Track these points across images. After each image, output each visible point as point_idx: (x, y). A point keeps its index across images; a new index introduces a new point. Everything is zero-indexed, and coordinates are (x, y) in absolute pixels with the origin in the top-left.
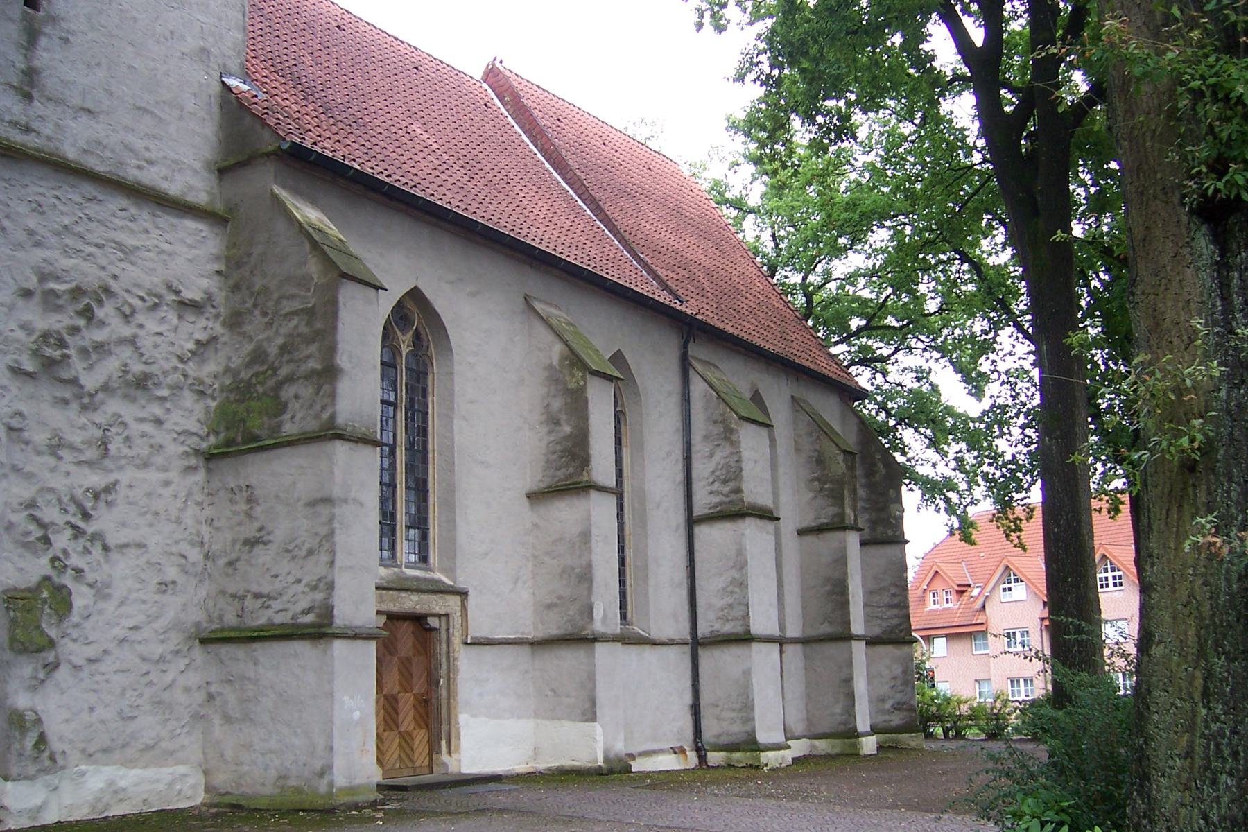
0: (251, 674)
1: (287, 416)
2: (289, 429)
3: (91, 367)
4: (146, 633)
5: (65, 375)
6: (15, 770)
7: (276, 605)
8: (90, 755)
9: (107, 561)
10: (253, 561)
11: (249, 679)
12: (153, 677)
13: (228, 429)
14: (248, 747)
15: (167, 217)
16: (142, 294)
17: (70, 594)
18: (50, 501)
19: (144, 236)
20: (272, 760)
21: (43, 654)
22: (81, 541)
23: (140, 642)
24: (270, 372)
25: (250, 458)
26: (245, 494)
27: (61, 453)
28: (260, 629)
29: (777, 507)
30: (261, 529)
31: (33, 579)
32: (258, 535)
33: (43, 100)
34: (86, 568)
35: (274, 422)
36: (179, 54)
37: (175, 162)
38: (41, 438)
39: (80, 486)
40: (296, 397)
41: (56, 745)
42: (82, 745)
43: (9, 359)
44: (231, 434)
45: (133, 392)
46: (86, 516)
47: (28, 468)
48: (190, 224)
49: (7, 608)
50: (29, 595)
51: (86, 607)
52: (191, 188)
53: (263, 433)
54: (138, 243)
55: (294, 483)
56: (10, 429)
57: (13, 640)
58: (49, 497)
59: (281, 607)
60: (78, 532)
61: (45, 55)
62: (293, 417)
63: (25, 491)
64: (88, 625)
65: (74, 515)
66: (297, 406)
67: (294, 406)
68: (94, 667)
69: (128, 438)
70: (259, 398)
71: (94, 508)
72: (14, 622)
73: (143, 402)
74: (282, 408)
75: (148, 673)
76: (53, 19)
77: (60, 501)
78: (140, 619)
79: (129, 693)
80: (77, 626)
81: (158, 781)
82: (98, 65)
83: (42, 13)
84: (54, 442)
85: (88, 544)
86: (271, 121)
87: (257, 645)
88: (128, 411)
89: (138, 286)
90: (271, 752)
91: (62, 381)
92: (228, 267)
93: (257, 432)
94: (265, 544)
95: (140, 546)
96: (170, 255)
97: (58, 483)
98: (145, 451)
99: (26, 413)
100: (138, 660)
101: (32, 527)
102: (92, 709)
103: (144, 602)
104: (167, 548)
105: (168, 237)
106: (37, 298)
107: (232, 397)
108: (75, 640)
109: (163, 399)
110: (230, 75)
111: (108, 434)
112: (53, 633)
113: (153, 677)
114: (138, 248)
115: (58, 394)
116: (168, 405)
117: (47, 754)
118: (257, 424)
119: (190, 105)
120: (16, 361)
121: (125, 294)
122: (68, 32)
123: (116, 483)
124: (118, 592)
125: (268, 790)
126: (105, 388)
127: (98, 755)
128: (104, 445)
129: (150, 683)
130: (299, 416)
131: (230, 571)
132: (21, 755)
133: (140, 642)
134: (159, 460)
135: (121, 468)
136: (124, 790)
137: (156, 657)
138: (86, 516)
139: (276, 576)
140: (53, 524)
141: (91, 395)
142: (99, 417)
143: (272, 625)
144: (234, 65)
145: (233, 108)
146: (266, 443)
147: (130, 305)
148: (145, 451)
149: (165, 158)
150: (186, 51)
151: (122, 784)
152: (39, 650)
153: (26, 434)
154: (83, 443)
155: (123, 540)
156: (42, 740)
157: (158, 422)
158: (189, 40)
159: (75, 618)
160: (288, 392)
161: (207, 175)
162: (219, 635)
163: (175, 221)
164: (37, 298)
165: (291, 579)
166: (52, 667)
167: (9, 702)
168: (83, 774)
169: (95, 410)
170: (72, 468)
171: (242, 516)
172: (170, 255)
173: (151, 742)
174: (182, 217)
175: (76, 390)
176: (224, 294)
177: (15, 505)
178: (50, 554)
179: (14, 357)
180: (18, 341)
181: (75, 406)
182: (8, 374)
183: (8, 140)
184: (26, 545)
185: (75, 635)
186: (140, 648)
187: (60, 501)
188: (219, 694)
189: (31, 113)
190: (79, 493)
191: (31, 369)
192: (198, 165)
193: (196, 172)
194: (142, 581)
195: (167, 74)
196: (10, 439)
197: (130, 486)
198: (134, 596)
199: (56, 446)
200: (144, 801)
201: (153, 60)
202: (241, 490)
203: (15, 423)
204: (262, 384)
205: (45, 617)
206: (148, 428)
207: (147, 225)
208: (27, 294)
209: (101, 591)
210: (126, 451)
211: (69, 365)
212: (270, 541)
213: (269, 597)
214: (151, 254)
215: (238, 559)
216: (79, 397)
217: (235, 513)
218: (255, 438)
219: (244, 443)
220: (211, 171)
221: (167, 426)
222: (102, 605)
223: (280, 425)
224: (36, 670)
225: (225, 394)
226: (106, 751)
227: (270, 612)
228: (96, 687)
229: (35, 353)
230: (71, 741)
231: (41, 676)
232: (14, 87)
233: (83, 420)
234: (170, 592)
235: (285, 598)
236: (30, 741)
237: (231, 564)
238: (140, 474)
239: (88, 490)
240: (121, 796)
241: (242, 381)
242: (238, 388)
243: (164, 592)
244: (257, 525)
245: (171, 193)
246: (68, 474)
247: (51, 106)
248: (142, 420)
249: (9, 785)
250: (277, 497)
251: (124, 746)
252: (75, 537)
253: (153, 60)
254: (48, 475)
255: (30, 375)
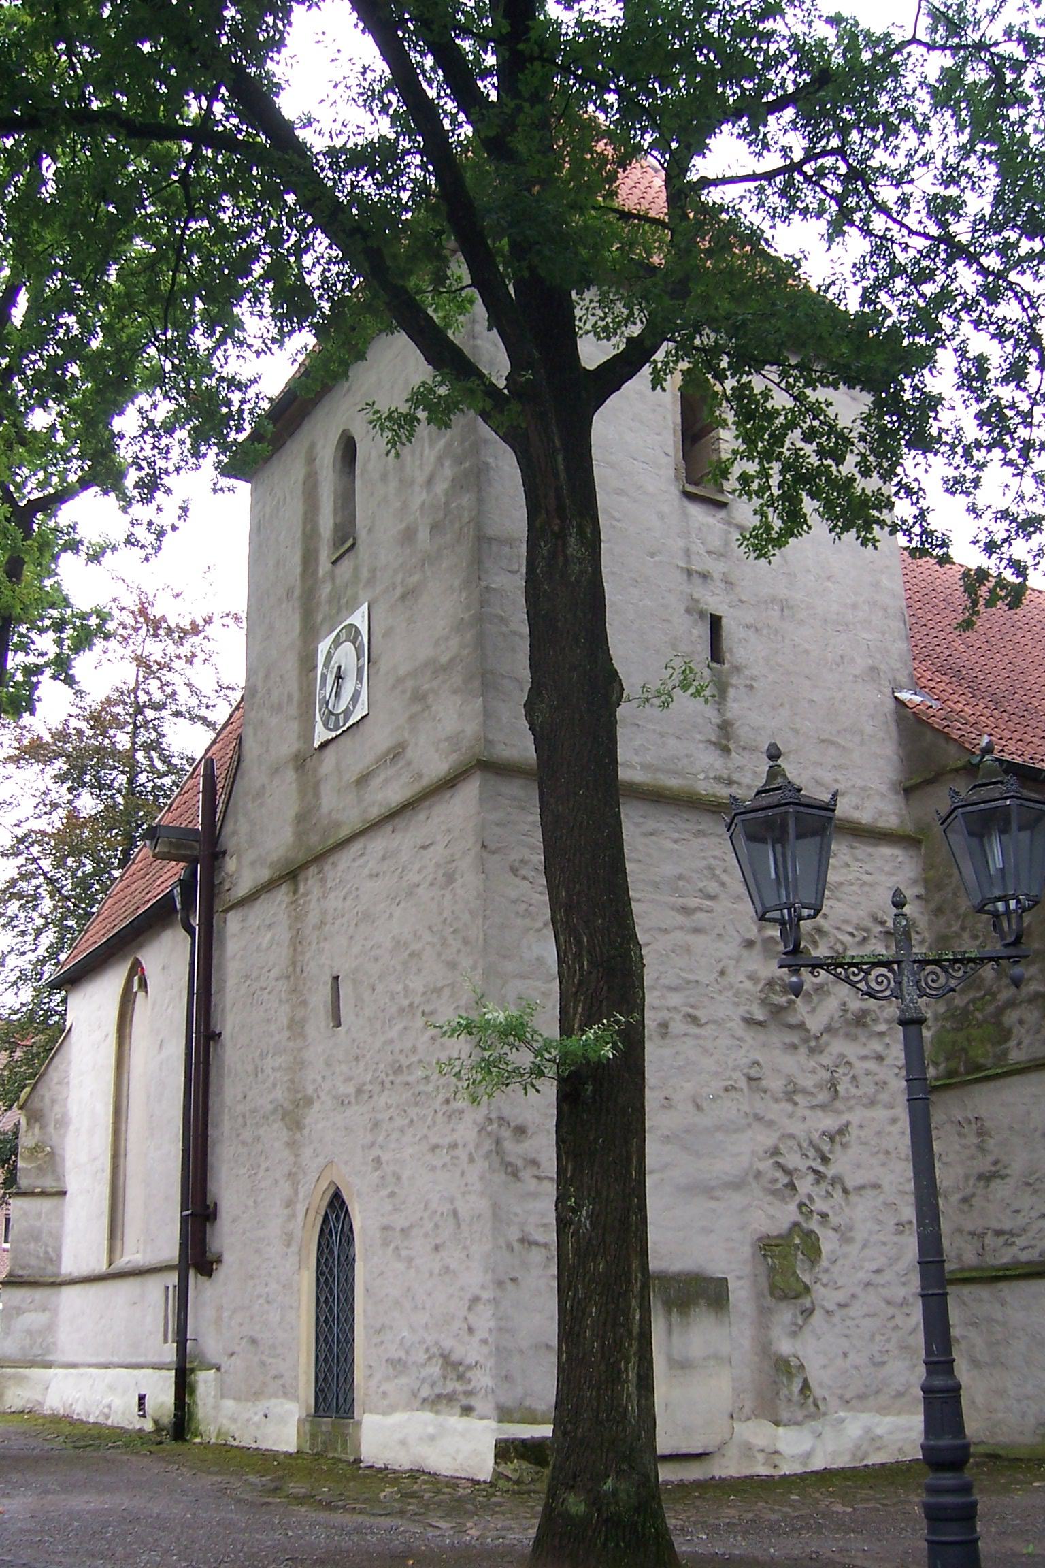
0: (999, 1316)
1: (1012, 1043)
2: (1016, 1056)
3: (814, 1010)
4: (888, 1276)
5: (793, 1020)
6: (785, 1415)
7: (1020, 1242)
8: (847, 1402)
9: (848, 1204)
10: (991, 1197)
11: (996, 1321)
12: (899, 1320)
13: (947, 1059)
14: (1001, 1393)
15: (863, 847)
16: (851, 930)
17: (818, 1239)
18: (791, 1148)
19: (844, 871)
20: (1028, 1406)
21: (800, 1301)
22: (824, 1185)
23: (883, 1286)
24: (988, 997)
25: (977, 1088)
26: (974, 1127)
27: (797, 1098)
28: (1005, 1267)
29: (684, 509)
30: (996, 1163)
31: (784, 1226)
32: (993, 1169)
33: (740, 751)
34: (830, 1214)
35: (999, 1049)
36: (851, 678)
37: (863, 789)
38: (776, 1084)
39: (817, 1131)
40: (1021, 1022)
41: (817, 1391)
42: (839, 1392)
43: (742, 1010)
44: (952, 1065)
45: (853, 1030)
46: (825, 1160)
47: (769, 1116)
48: (886, 851)
49: (764, 1255)
50: (781, 1242)
51: (833, 1252)
52: (881, 813)
53: (988, 1062)
54: (842, 879)
55: (1029, 1113)
56: (750, 1079)
57: (773, 1288)
58: (791, 1143)
59: (1026, 1244)
60: (819, 1176)
61: (736, 706)
62: (1019, 1044)
63: (767, 1139)
64: (835, 1269)
65: (814, 1159)
66: (1023, 1031)
67: (1019, 1031)
68: (844, 1312)
69: (854, 1078)
70: (979, 1025)
71: (831, 1152)
72: (772, 1269)
73: (864, 1040)
74: (1006, 1034)
75: (893, 1317)
76: (737, 669)
77: (800, 1146)
78: (881, 1262)
79: (878, 1337)
80: (827, 1271)
81: (910, 1429)
82: (782, 705)
83: (726, 666)
84: (791, 1088)
85: (830, 1188)
86: (955, 735)
87: (1001, 1285)
88: (851, 1050)
89: (846, 922)
90: (1028, 1398)
91: (791, 1027)
92: (926, 889)
93: (982, 1061)
94: (1003, 1177)
95: (876, 1186)
96: (871, 885)
97: (797, 1128)
98: (871, 1090)
99: (761, 1061)
100: (883, 1305)
101: (779, 1174)
102: (845, 1355)
103: (884, 1244)
104: (901, 1187)
105: (867, 867)
106: (758, 947)
107: (948, 1025)
108: (825, 1285)
109: (881, 1034)
110: (901, 689)
111: (836, 1075)
112: (806, 1278)
113: (899, 1320)
114: (841, 884)
115: (787, 1040)
116: (887, 1040)
117: (811, 1399)
118: (982, 1053)
119: (869, 729)
120: (749, 1012)
121: (836, 932)
122: (752, 679)
123: (848, 1124)
124: (859, 1236)
125: (1028, 1439)
126: (829, 1029)
127: (854, 1402)
128: (833, 1085)
129: (897, 1327)
130: (1026, 1041)
131: (966, 1208)
132: (789, 1400)
133: (883, 1286)
134: (884, 1097)
135: (850, 1109)
136: (880, 1437)
137: (899, 1300)
138: (825, 1160)
139: (1018, 1211)
140: (796, 1169)
141: (817, 1038)
142: (826, 1059)
143: (1017, 1264)
144: (903, 678)
145: (912, 726)
146: (992, 1072)
147: (842, 943)
148: (871, 1090)
149: (853, 786)
150: (857, 672)
151: (879, 1431)
152: (797, 1297)
153: (764, 1083)
154: (815, 1086)
155: (860, 1182)
156: (806, 1386)
157: (880, 1058)
158: (859, 661)
159: (824, 1263)
160: (1011, 1017)
161: (894, 797)
162: (959, 1276)
163: (870, 850)
164: (758, 947)
165: (1034, 1214)
166: (808, 1313)
167: (773, 1348)
168: (842, 1421)
169: (822, 1052)
170: (807, 1113)
171: (973, 1150)
172: (871, 885)
173: (902, 1389)
174: (876, 845)
175: (803, 1034)
176: (926, 918)
177: (761, 1153)
178: (797, 1200)
179: (747, 1007)
180: (747, 991)
181: (803, 1050)
182: (742, 1024)
183: (715, 796)
184: (774, 1193)
185: (825, 1281)
186: (885, 1292)
187: (800, 1146)
188: (964, 1337)
189: (730, 765)
190: (816, 1136)
191: (761, 1018)
192: (883, 788)
193: (883, 795)
194: (880, 1222)
195: (843, 701)
196: (750, 1088)
197: (861, 1126)
198: (875, 1237)
199: (792, 1092)
200: (900, 1450)
201: (829, 689)
202: (970, 1122)
203: (753, 1072)
204: (981, 1010)
205: (798, 1263)
206: (871, 1065)
207: (847, 858)
208: (750, 944)
209: (844, 1234)
210: (853, 1091)
211: (795, 1010)
212: (1007, 1175)
213: (1011, 1233)
214: (854, 888)
215: (973, 1195)
216: (806, 1041)
217: (964, 1147)
218: (979, 1068)
219: (968, 1073)
220: (897, 793)
221: (888, 1061)
222: (846, 1248)
223: (1005, 1053)
224: (794, 1316)
225: (939, 1023)
226: (861, 1397)
227: (1015, 1250)
228: (847, 1332)
229: (764, 1002)
230: (830, 1387)
231: (800, 1322)
232: (714, 743)
233: (812, 1063)
234: (907, 1232)
235: (1030, 1234)
236: (796, 1386)
237: (965, 1200)
238: (869, 1113)
239: (824, 1134)
240: (878, 1444)
241: (957, 1008)
242: (954, 1016)
243: (902, 1232)
244: (990, 1159)
245: (863, 822)
246: (804, 1118)
247: (746, 754)
248: (864, 1058)
249: (781, 1429)
250: (1011, 1128)
251: (877, 1392)
252: (818, 1182)
253: (829, 689)
254: (786, 1121)
255: (760, 1024)
